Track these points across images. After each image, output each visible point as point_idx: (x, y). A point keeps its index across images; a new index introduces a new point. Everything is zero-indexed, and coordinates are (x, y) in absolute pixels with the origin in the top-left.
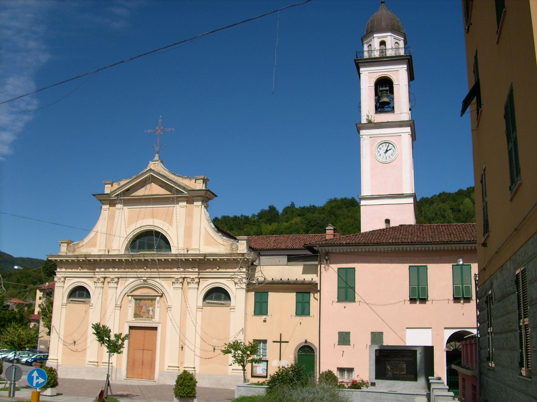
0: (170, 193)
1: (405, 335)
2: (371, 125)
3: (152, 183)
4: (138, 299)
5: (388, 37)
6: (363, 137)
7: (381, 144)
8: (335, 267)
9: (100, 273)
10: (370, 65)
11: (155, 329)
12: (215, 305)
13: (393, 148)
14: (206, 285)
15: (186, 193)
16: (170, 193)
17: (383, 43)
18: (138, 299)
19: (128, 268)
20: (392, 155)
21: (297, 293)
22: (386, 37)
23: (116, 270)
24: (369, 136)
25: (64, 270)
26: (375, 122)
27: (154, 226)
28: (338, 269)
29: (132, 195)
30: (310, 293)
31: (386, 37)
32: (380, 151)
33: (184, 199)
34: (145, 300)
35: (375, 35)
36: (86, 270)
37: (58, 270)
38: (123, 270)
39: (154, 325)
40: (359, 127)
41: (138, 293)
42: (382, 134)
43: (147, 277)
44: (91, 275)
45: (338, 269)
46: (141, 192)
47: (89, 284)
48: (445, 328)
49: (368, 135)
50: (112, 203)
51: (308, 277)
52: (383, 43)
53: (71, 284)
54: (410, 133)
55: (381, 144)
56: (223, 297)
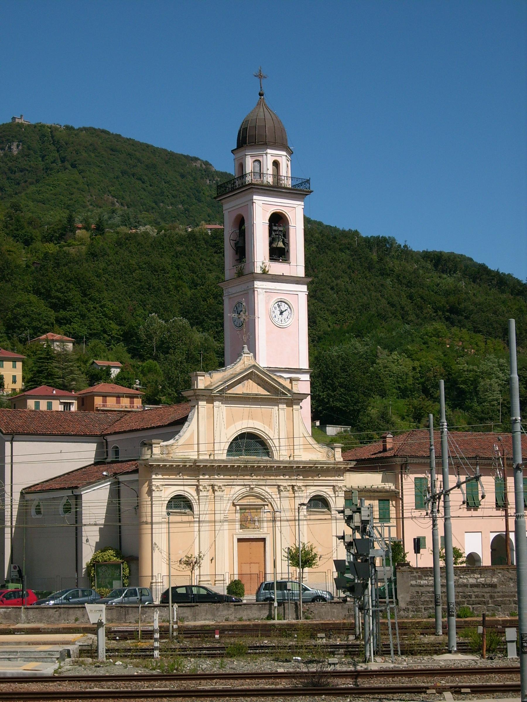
0: (269, 394)
1: (463, 539)
2: (265, 276)
3: (249, 380)
4: (244, 508)
5: (283, 157)
6: (258, 290)
7: (281, 301)
8: (412, 477)
9: (205, 481)
10: (265, 193)
11: (264, 540)
12: (318, 513)
13: (289, 309)
14: (312, 491)
15: (289, 395)
16: (269, 394)
17: (276, 164)
18: (244, 508)
19: (234, 475)
20: (287, 318)
21: (379, 500)
22: (280, 156)
23: (222, 477)
24: (265, 290)
25: (160, 477)
26: (269, 273)
27: (255, 428)
28: (415, 478)
29: (228, 392)
30: (389, 500)
31: (280, 156)
32: (275, 310)
33: (285, 401)
34: (250, 509)
35: (269, 151)
36: (186, 477)
37: (154, 477)
38: (262, 478)
39: (262, 536)
40: (254, 277)
41: (244, 502)
42: (284, 290)
43: (256, 485)
44: (195, 482)
45: (415, 478)
46: (239, 390)
47: (190, 492)
48: (491, 532)
49: (264, 289)
50: (211, 400)
51: (390, 486)
52: (276, 164)
53: (169, 493)
54: (307, 293)
55: (281, 301)
56: (320, 505)
